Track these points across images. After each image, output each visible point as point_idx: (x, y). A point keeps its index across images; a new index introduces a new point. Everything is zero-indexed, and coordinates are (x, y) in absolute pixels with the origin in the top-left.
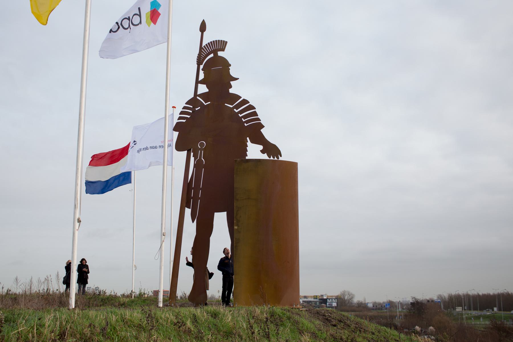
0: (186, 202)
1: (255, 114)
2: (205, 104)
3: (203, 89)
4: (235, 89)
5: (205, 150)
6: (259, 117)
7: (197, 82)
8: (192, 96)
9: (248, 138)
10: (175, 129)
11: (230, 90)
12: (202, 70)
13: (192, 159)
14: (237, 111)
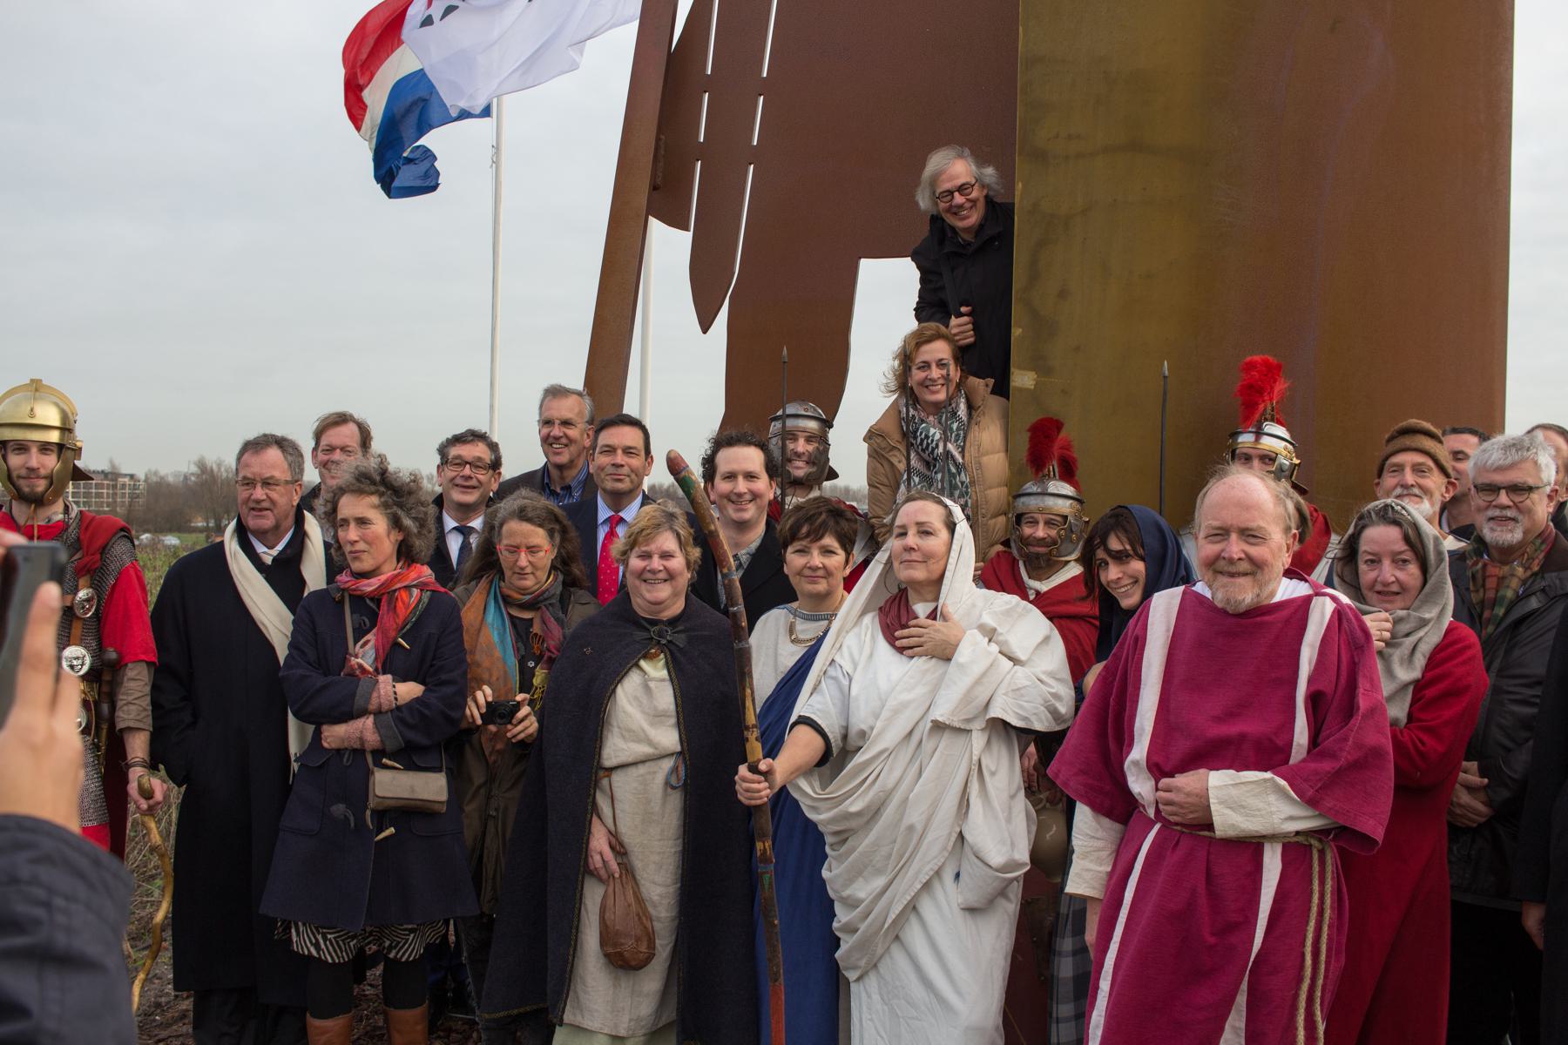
0: (658, 173)
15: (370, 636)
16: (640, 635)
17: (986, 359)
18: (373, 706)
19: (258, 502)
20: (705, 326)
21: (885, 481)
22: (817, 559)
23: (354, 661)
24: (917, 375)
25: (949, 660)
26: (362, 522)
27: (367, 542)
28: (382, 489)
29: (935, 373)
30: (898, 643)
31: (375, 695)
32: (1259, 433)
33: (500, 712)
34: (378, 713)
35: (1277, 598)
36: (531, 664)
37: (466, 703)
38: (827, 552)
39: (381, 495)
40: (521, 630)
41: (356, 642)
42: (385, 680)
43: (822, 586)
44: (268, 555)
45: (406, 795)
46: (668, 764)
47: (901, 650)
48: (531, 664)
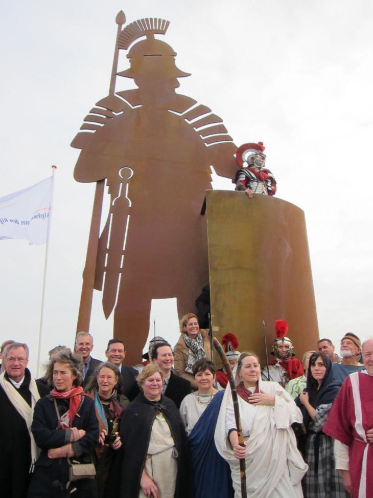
0: (94, 275)
1: (223, 129)
2: (133, 108)
3: (127, 84)
4: (184, 88)
5: (132, 182)
6: (225, 123)
7: (115, 74)
9: (212, 167)
15: (67, 413)
16: (152, 407)
17: (205, 323)
18: (71, 440)
19: (16, 366)
20: (107, 316)
21: (181, 359)
22: (204, 377)
23: (62, 423)
24: (189, 327)
25: (273, 405)
26: (63, 372)
27: (64, 380)
28: (70, 361)
29: (194, 326)
30: (250, 401)
31: (72, 435)
32: (283, 340)
33: (110, 439)
34: (73, 443)
35: (248, 389)
36: (111, 421)
37: (99, 438)
38: (208, 374)
39: (70, 363)
40: (106, 408)
41: (61, 416)
42: (75, 429)
43: (207, 386)
44: (18, 385)
45: (83, 474)
46: (171, 451)
47: (252, 403)
48: (111, 421)
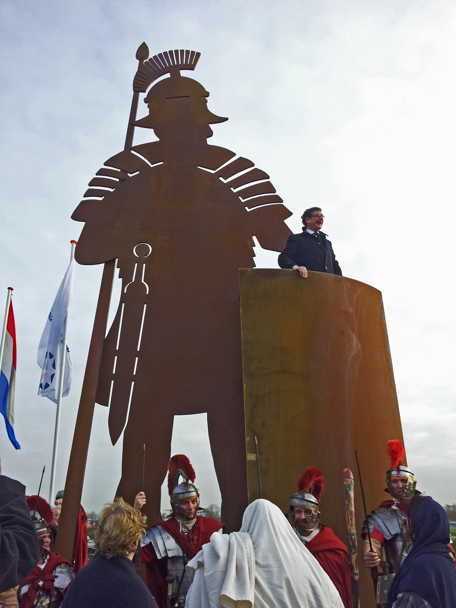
1: (270, 188)
3: (145, 136)
5: (150, 261)
8: (121, 148)
9: (254, 238)
10: (76, 216)
11: (208, 140)
12: (146, 101)
13: (117, 283)
14: (235, 191)
